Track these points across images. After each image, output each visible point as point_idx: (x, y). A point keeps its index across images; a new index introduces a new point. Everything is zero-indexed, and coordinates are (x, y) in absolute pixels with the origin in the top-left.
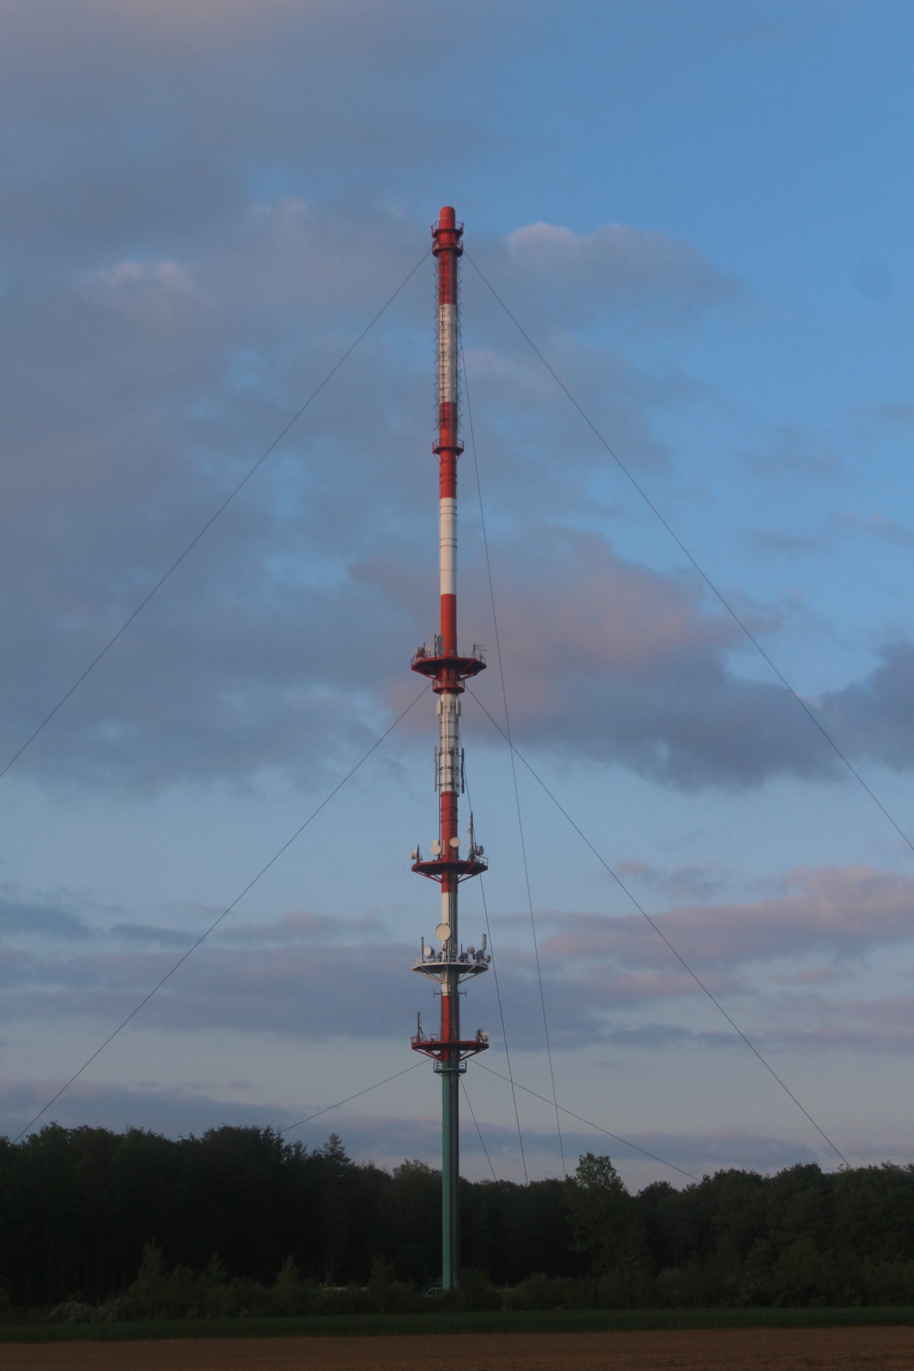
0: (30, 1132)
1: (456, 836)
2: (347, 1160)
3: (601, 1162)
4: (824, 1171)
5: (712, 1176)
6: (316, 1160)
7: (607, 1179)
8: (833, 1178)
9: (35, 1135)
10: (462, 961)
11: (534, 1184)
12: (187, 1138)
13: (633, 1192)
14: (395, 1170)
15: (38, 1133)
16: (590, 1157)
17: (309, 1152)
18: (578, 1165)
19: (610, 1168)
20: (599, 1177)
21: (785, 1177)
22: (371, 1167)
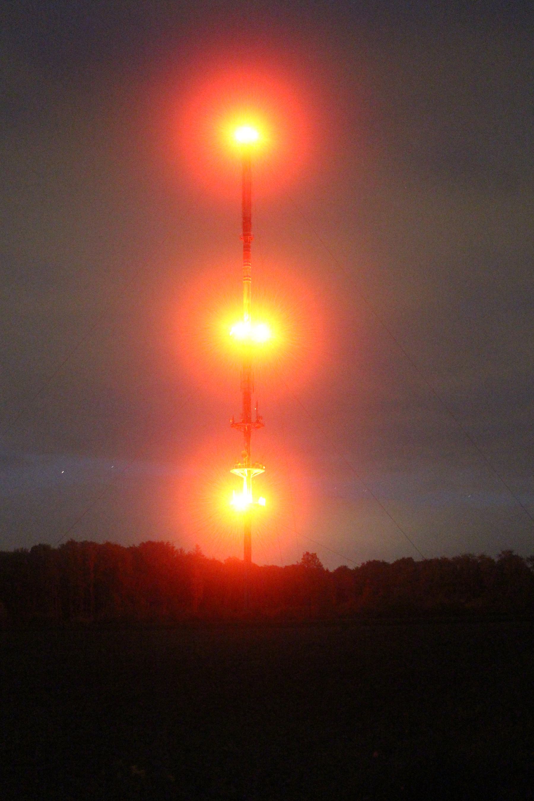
0: (60, 543)
1: (315, 554)
2: (203, 556)
3: (312, 556)
4: (331, 570)
5: (366, 563)
6: (189, 556)
7: (315, 563)
8: (419, 563)
9: (63, 545)
10: (250, 471)
11: (286, 567)
12: (131, 546)
13: (496, 560)
14: (225, 561)
15: (65, 543)
16: (308, 553)
17: (186, 552)
18: (302, 557)
19: (316, 558)
20: (311, 562)
21: (398, 563)
22: (214, 559)
